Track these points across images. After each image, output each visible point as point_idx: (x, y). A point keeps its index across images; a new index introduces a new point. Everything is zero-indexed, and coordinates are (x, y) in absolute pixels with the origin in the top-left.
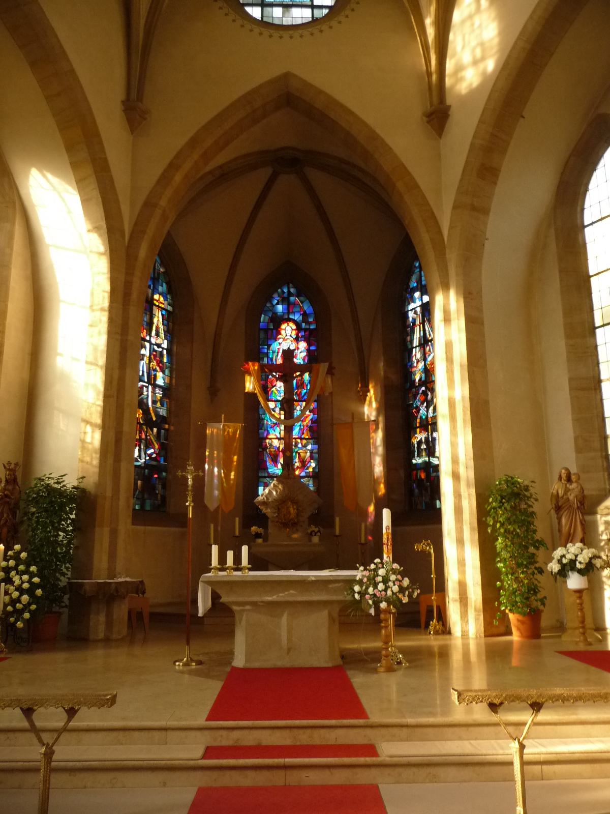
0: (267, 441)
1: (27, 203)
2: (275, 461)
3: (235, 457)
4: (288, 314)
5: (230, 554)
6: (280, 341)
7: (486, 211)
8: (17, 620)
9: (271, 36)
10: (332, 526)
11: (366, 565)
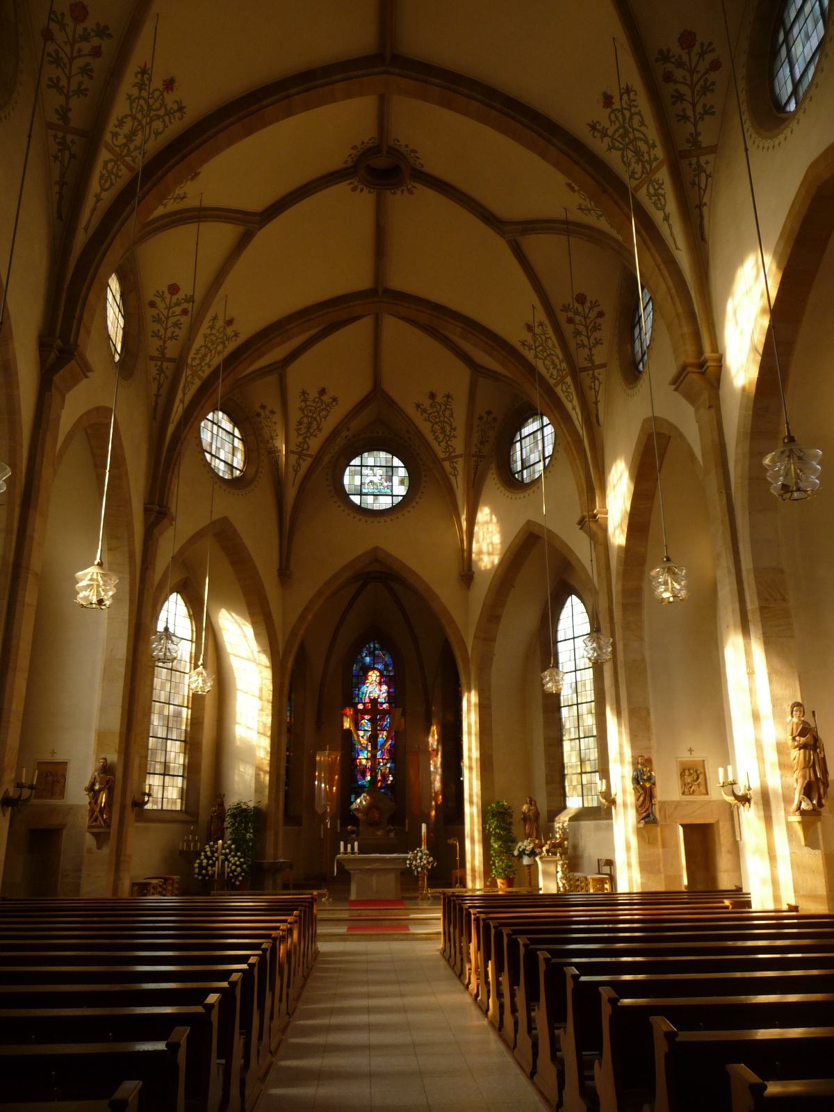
0: (358, 760)
1: (216, 628)
2: (364, 776)
3: (337, 777)
5: (349, 846)
6: (368, 685)
7: (493, 640)
11: (413, 851)
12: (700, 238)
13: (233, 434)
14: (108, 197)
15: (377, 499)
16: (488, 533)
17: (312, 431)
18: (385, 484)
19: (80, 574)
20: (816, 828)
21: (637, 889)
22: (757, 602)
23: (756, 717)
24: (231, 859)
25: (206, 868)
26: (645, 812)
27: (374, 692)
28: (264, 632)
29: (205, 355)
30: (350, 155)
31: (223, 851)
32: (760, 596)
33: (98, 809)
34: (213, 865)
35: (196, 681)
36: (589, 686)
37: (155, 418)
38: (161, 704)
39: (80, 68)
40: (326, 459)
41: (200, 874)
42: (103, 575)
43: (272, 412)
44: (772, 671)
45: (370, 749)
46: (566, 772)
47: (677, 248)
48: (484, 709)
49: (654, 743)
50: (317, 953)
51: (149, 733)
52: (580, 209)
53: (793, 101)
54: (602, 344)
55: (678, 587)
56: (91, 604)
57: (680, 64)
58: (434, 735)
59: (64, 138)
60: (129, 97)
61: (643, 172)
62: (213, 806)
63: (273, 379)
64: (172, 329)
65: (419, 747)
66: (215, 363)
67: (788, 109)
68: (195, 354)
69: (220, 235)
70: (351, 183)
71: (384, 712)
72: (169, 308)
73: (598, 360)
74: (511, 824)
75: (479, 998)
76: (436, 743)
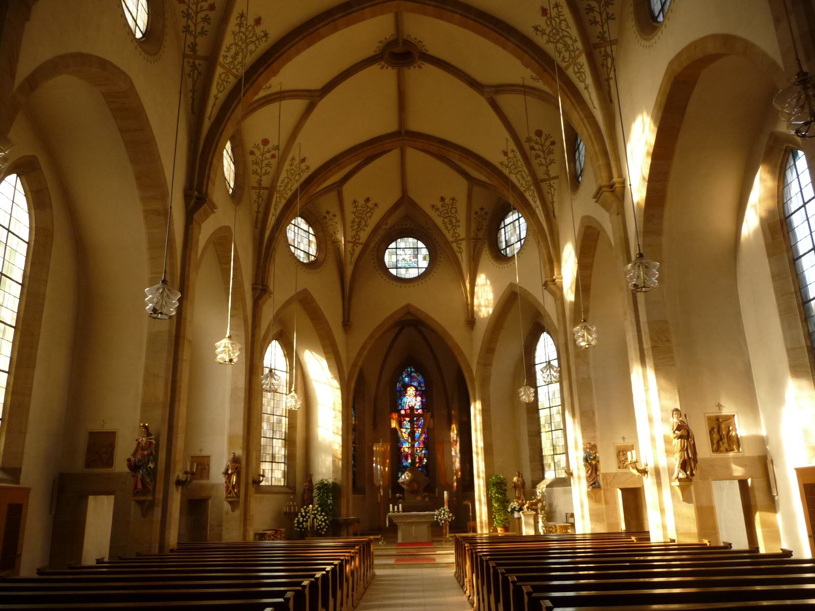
0: (402, 449)
1: (302, 362)
2: (407, 460)
3: (388, 461)
4: (411, 382)
5: (396, 507)
6: (407, 397)
7: (490, 365)
8: (322, 531)
9: (401, 287)
10: (435, 492)
12: (609, 100)
13: (308, 232)
14: (222, 96)
15: (408, 270)
16: (484, 292)
17: (361, 227)
18: (413, 260)
19: (218, 344)
20: (690, 491)
21: (588, 531)
22: (649, 343)
23: (650, 420)
24: (318, 517)
25: (302, 523)
26: (592, 481)
27: (411, 402)
28: (335, 365)
29: (288, 183)
30: (378, 47)
31: (313, 512)
32: (652, 339)
33: (231, 486)
34: (307, 521)
35: (292, 401)
36: (558, 395)
37: (256, 227)
38: (268, 415)
39: (201, 18)
40: (372, 245)
41: (298, 527)
42: (232, 344)
43: (334, 216)
44: (660, 389)
45: (410, 441)
46: (544, 454)
47: (594, 108)
48: (485, 412)
49: (598, 434)
50: (374, 575)
51: (261, 435)
52: (532, 78)
53: (661, 15)
54: (554, 163)
55: (591, 339)
56: (226, 362)
57: (537, 143)
58: (454, 431)
59: (194, 63)
60: (233, 32)
61: (570, 58)
62: (305, 482)
63: (333, 195)
64: (265, 168)
65: (443, 439)
66: (294, 187)
67: (659, 20)
68: (281, 183)
69: (296, 106)
70: (379, 64)
71: (419, 416)
72: (263, 155)
73: (552, 174)
74: (506, 490)
75: (470, 598)
76: (455, 436)
